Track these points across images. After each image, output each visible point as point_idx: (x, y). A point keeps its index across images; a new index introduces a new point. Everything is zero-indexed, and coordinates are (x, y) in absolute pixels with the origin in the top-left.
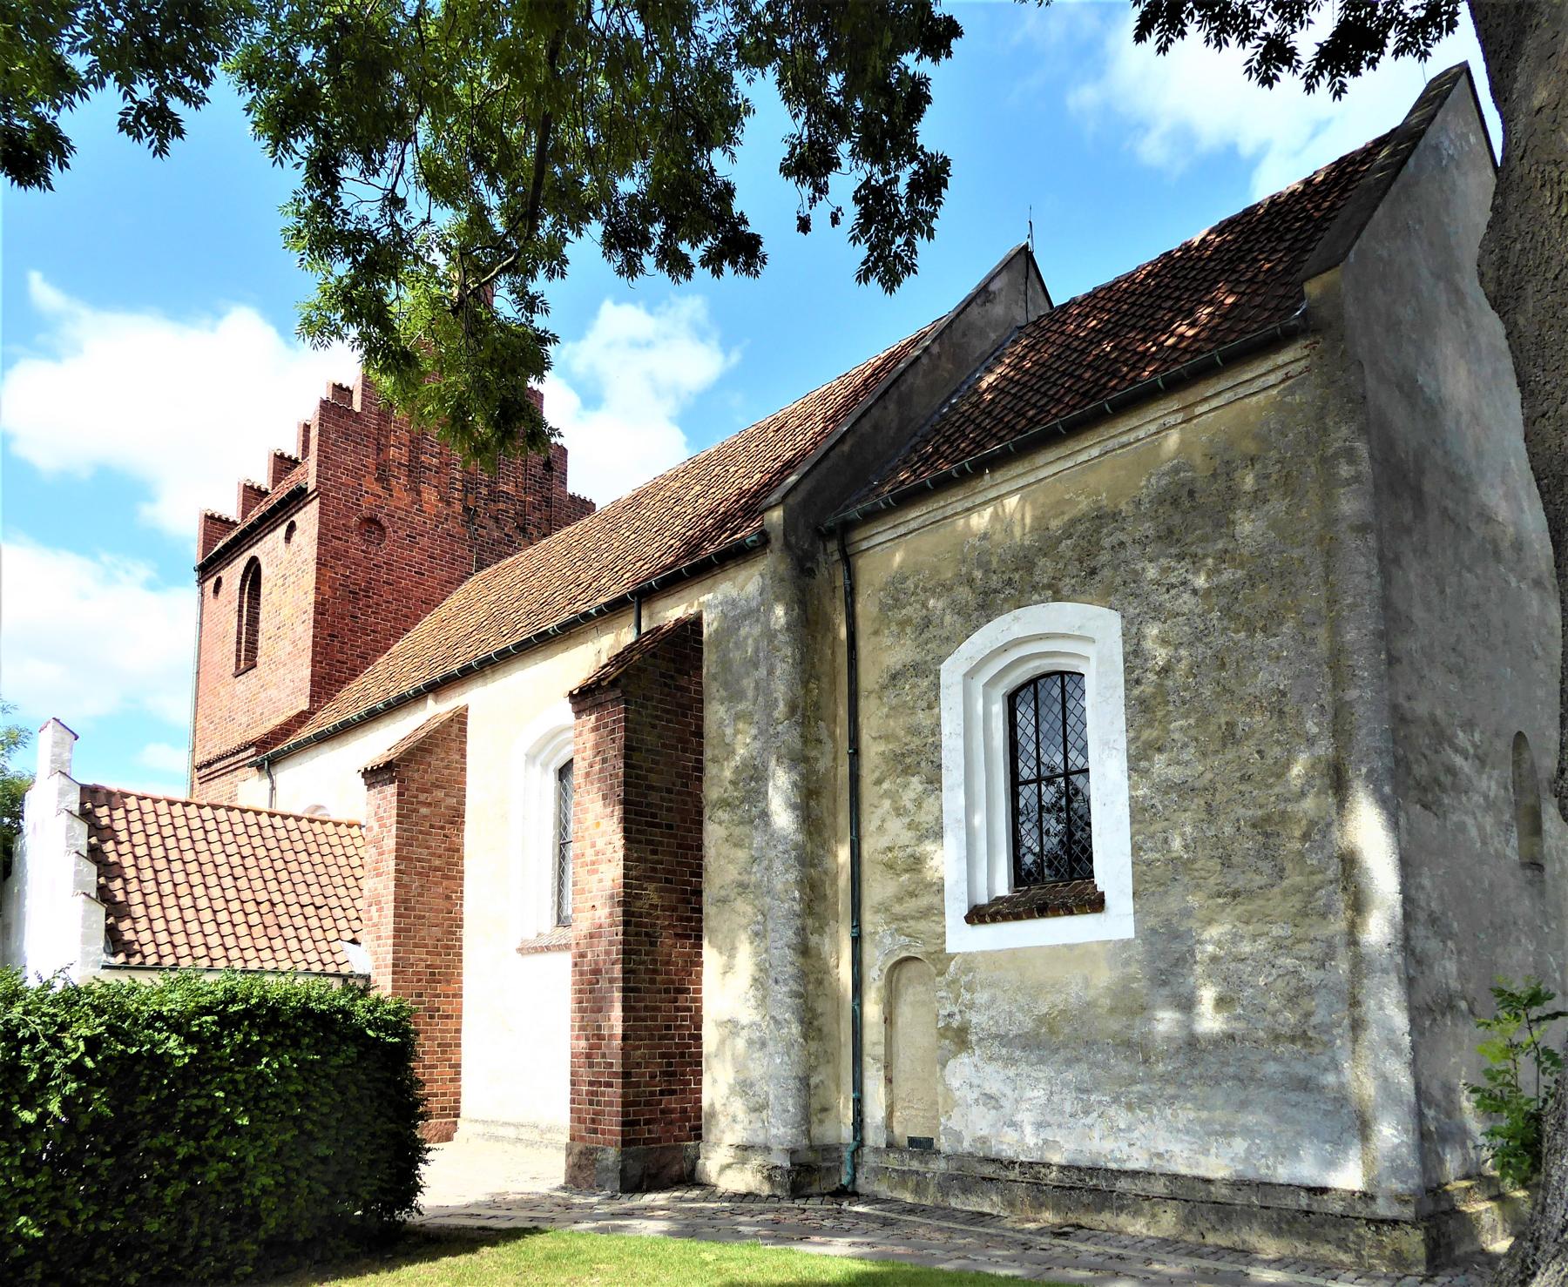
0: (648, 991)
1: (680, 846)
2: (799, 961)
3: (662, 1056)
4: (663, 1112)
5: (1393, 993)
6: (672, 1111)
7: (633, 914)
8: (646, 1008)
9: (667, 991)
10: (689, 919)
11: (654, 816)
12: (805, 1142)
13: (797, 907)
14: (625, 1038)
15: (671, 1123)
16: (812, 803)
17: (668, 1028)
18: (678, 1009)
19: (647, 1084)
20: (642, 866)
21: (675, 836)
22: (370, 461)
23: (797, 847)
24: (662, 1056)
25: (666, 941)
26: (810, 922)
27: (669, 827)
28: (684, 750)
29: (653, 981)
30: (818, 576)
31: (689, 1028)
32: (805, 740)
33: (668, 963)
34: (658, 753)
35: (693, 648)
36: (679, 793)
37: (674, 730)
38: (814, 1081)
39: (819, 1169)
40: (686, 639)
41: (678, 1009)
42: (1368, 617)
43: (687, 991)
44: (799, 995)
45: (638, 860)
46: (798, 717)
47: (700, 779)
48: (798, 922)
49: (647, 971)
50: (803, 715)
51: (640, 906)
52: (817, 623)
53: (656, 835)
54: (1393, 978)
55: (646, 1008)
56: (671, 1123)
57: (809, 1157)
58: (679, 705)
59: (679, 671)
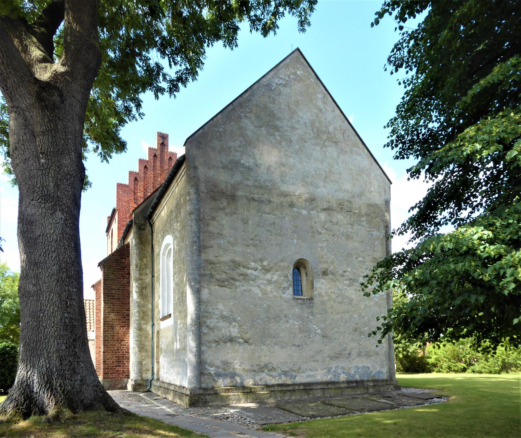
0: (111, 341)
1: (122, 304)
2: (138, 332)
3: (116, 357)
4: (116, 371)
5: (191, 337)
6: (120, 371)
7: (106, 322)
8: (111, 345)
9: (118, 341)
10: (125, 322)
11: (114, 296)
12: (140, 378)
13: (137, 318)
14: (104, 352)
15: (119, 374)
16: (144, 291)
17: (118, 350)
18: (121, 345)
19: (111, 364)
20: (109, 309)
21: (121, 301)
22: (132, 198)
23: (137, 302)
24: (116, 357)
25: (117, 328)
26: (142, 322)
27: (119, 299)
28: (123, 279)
29: (113, 338)
30: (147, 230)
31: (125, 350)
32: (141, 274)
33: (118, 334)
34: (114, 280)
35: (126, 252)
36: (122, 290)
37: (120, 274)
38: (144, 363)
39: (143, 385)
40: (124, 250)
41: (121, 345)
42: (190, 237)
43: (125, 340)
44: (138, 341)
45: (108, 308)
46: (138, 268)
47: (129, 286)
48: (138, 322)
49: (111, 336)
50: (140, 268)
51: (109, 319)
52: (146, 243)
53: (114, 301)
54: (191, 333)
55: (111, 345)
56: (119, 374)
57: (141, 382)
58: (122, 267)
59: (121, 258)
